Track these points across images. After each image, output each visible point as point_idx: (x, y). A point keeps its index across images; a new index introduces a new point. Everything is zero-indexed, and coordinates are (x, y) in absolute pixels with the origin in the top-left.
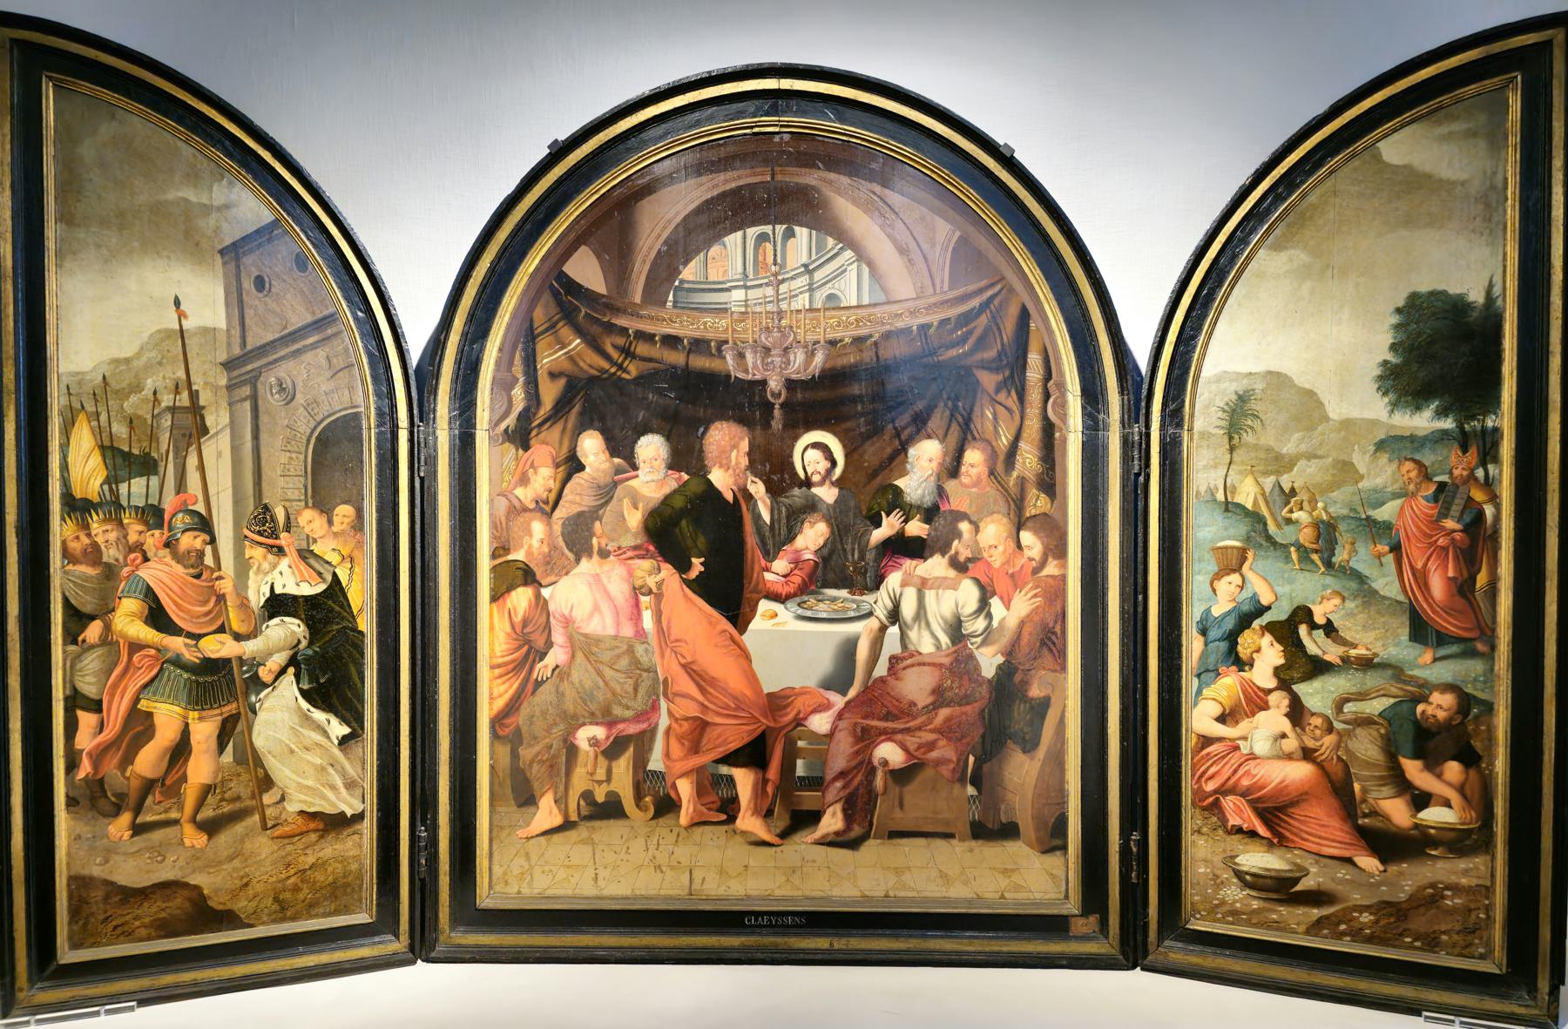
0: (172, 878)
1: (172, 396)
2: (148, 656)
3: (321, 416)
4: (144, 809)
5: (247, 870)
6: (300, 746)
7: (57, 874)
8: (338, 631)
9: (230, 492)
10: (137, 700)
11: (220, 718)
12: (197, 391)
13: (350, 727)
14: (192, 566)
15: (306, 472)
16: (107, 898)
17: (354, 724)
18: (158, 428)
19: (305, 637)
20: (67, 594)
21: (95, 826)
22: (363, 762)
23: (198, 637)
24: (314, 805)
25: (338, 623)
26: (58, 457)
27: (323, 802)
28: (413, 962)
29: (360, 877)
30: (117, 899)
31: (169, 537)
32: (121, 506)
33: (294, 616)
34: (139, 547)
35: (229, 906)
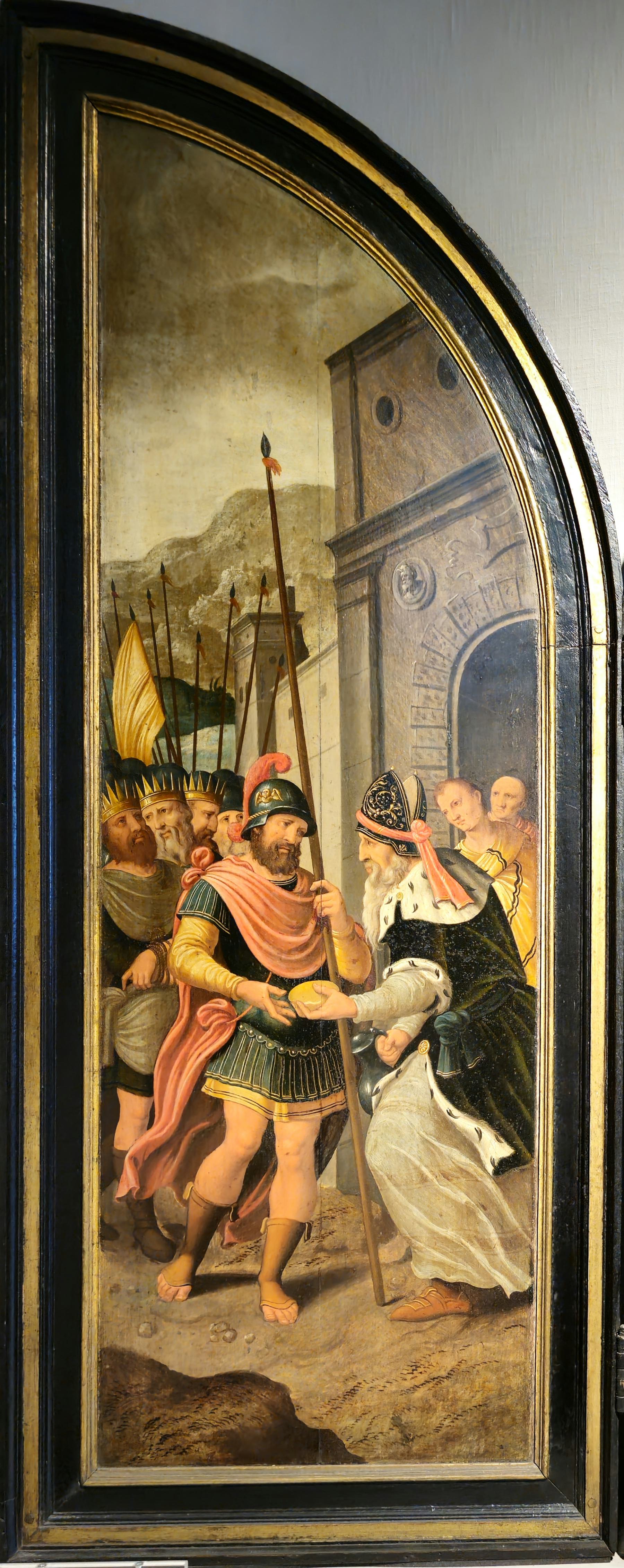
0: (245, 1368)
1: (256, 597)
2: (218, 1010)
3: (473, 628)
4: (207, 1254)
5: (354, 1368)
6: (436, 1171)
7: (84, 1344)
8: (497, 985)
9: (337, 752)
10: (201, 1080)
11: (318, 1116)
12: (292, 589)
13: (510, 1143)
14: (282, 871)
15: (450, 721)
16: (153, 1388)
17: (519, 1142)
18: (236, 648)
19: (445, 993)
20: (108, 907)
21: (139, 1273)
22: (532, 1206)
23: (288, 984)
24: (455, 1271)
25: (496, 973)
26: (97, 694)
27: (469, 1268)
28: (608, 1558)
29: (524, 1398)
30: (167, 1392)
31: (250, 823)
32: (183, 772)
33: (430, 958)
34: (206, 838)
35: (327, 1424)
